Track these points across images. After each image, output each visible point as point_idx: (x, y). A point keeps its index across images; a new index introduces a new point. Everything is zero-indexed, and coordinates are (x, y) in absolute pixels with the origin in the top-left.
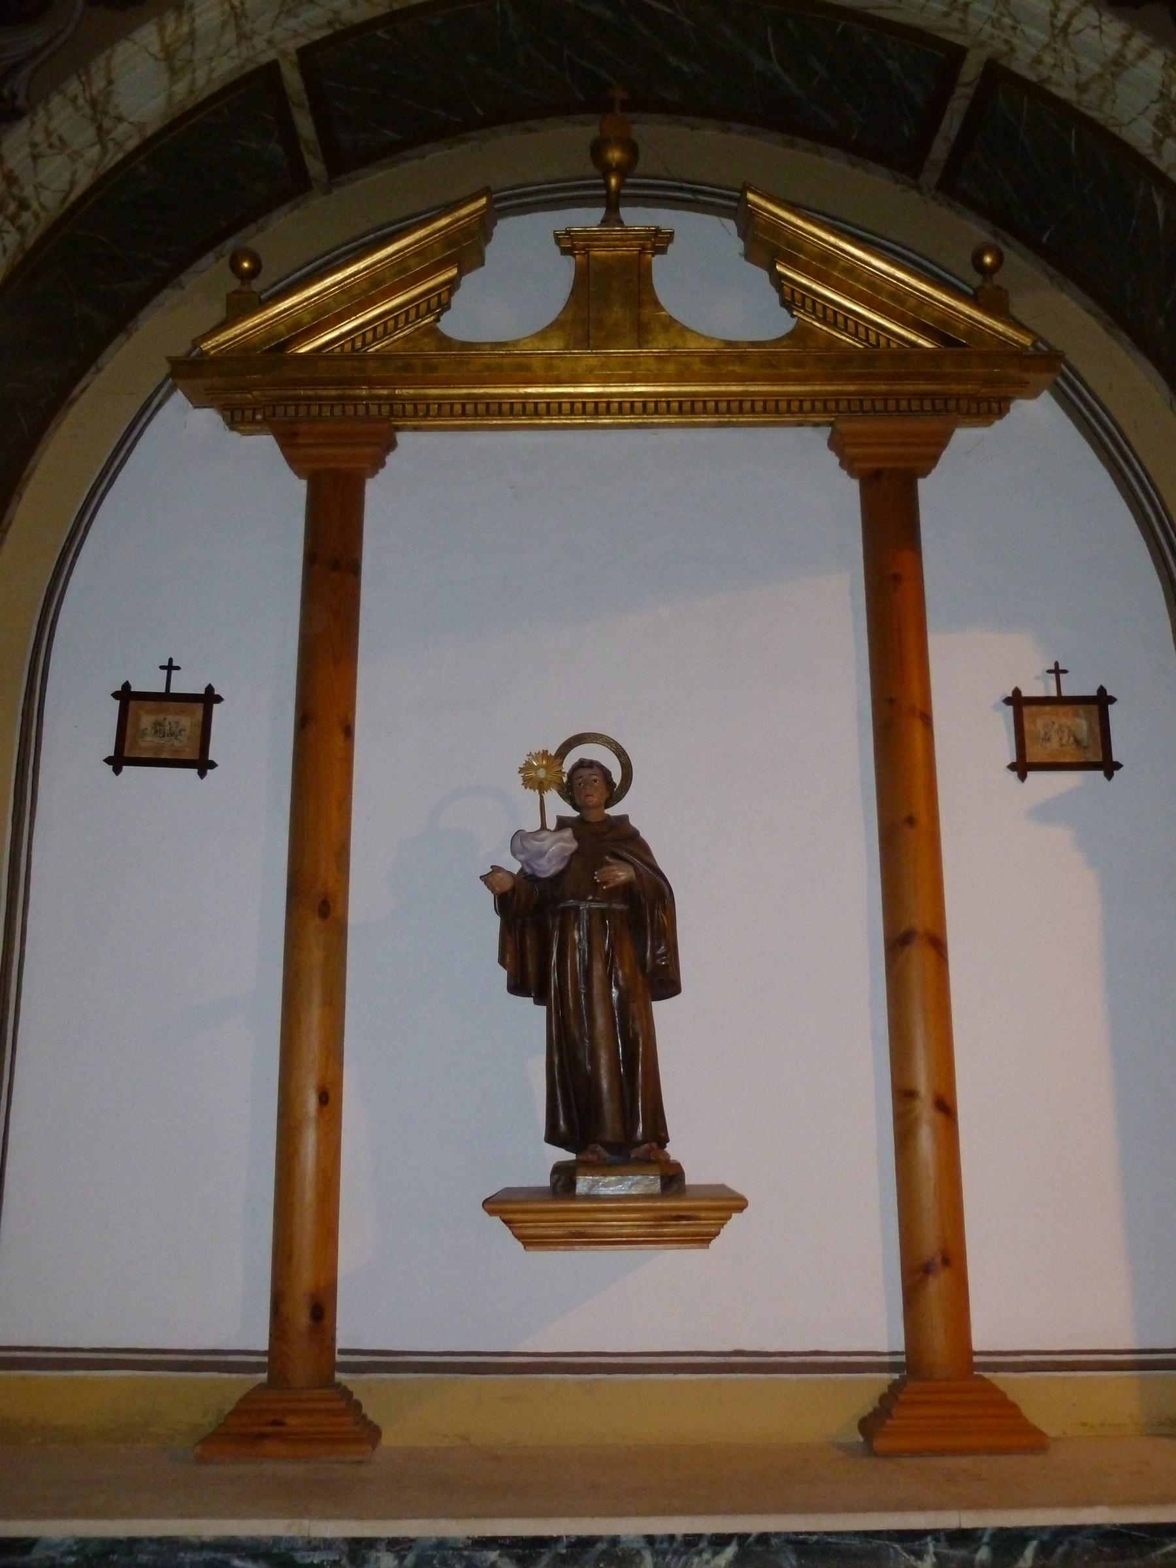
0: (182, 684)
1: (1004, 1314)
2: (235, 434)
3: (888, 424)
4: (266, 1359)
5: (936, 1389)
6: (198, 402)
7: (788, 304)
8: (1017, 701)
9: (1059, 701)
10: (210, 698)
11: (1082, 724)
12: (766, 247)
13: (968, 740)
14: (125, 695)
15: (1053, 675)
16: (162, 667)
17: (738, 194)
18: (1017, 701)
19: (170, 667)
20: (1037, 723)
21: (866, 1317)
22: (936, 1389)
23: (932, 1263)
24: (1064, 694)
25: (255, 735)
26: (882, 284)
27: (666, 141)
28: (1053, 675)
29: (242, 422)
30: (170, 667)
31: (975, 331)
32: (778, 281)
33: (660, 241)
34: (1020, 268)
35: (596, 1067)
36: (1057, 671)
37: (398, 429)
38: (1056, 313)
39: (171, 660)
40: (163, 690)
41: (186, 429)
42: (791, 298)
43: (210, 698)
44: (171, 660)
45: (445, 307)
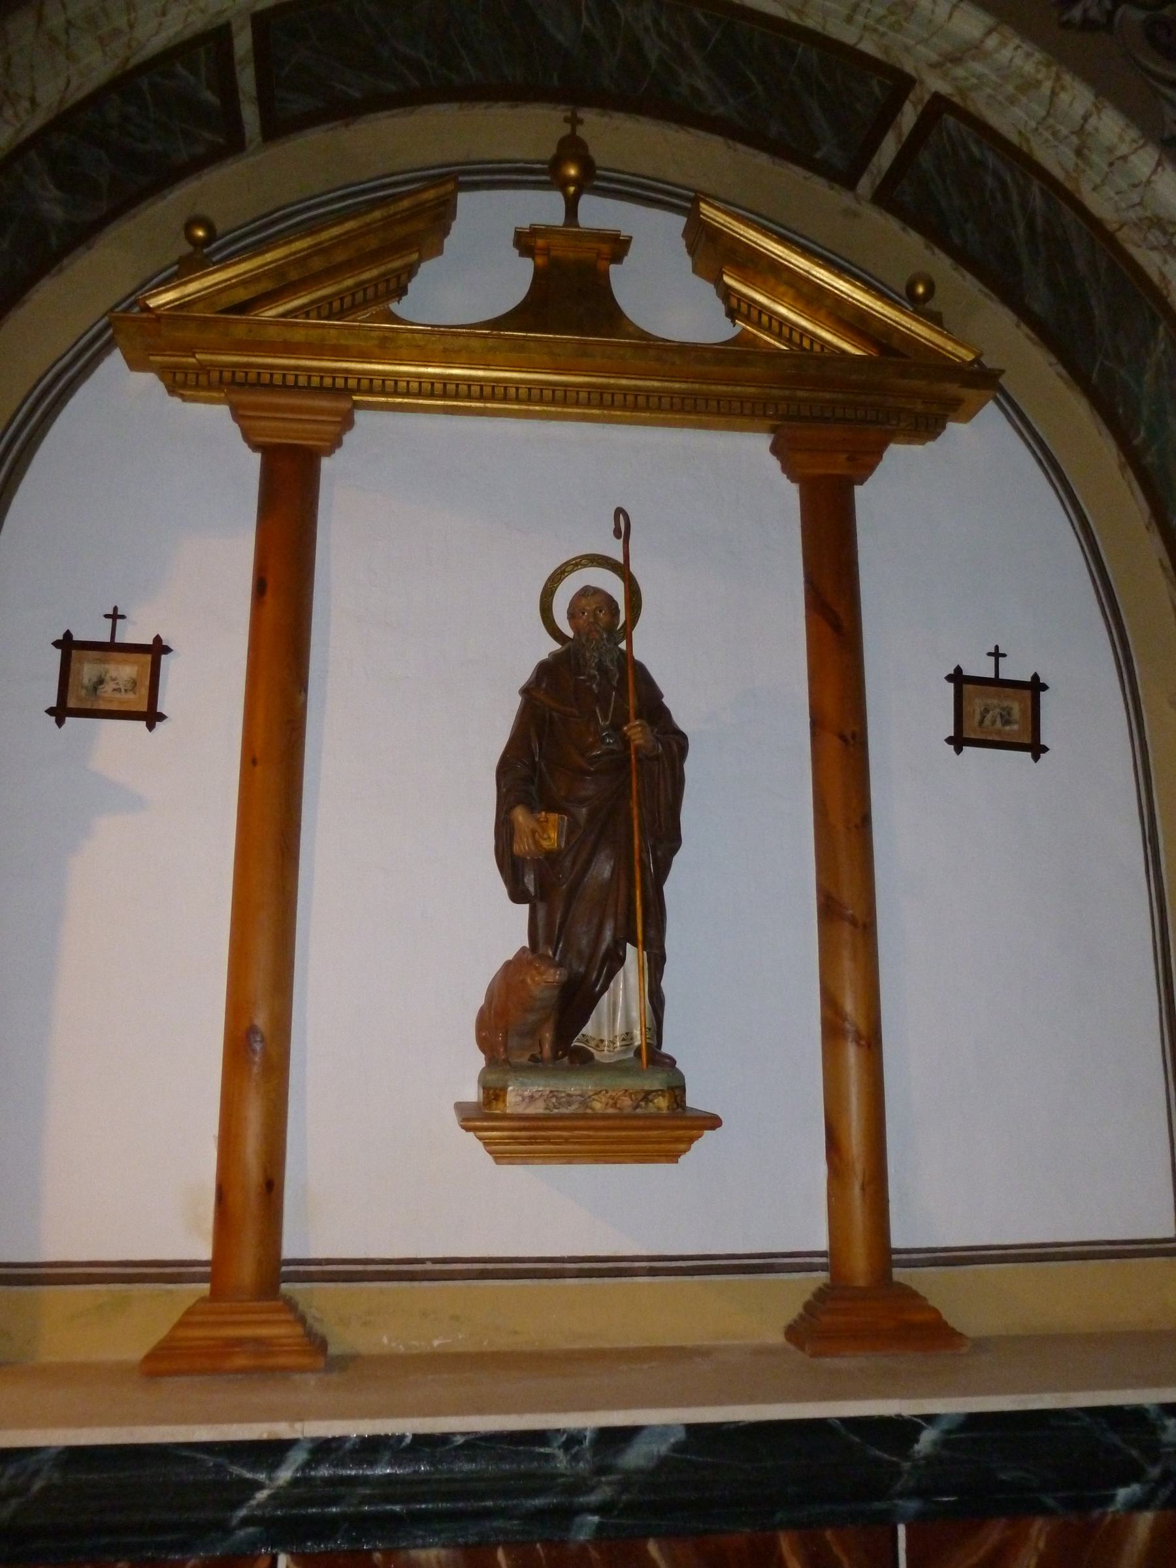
0: (129, 634)
1: (931, 1209)
2: (177, 400)
3: (835, 420)
4: (208, 1269)
5: (867, 1295)
6: (135, 364)
7: (732, 314)
8: (957, 678)
9: (996, 682)
10: (158, 649)
11: (1017, 706)
12: (712, 252)
13: (906, 712)
14: (67, 644)
15: (993, 658)
16: (107, 616)
17: (689, 205)
18: (957, 678)
19: (115, 616)
20: (976, 703)
21: (802, 1222)
22: (867, 1295)
23: (859, 1163)
24: (1001, 677)
25: (209, 684)
26: (829, 287)
27: (614, 137)
28: (993, 658)
29: (185, 385)
30: (115, 616)
31: (910, 340)
32: (726, 293)
33: (618, 246)
34: (958, 285)
35: (780, 326)
36: (997, 654)
37: (357, 405)
38: (989, 330)
39: (115, 609)
40: (108, 640)
41: (120, 390)
42: (735, 307)
43: (158, 649)
44: (115, 609)
45: (401, 291)
